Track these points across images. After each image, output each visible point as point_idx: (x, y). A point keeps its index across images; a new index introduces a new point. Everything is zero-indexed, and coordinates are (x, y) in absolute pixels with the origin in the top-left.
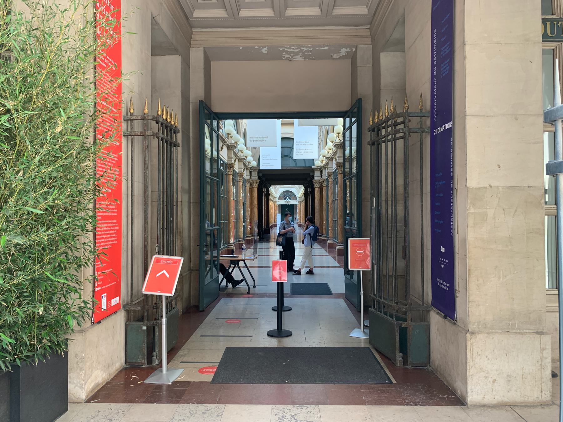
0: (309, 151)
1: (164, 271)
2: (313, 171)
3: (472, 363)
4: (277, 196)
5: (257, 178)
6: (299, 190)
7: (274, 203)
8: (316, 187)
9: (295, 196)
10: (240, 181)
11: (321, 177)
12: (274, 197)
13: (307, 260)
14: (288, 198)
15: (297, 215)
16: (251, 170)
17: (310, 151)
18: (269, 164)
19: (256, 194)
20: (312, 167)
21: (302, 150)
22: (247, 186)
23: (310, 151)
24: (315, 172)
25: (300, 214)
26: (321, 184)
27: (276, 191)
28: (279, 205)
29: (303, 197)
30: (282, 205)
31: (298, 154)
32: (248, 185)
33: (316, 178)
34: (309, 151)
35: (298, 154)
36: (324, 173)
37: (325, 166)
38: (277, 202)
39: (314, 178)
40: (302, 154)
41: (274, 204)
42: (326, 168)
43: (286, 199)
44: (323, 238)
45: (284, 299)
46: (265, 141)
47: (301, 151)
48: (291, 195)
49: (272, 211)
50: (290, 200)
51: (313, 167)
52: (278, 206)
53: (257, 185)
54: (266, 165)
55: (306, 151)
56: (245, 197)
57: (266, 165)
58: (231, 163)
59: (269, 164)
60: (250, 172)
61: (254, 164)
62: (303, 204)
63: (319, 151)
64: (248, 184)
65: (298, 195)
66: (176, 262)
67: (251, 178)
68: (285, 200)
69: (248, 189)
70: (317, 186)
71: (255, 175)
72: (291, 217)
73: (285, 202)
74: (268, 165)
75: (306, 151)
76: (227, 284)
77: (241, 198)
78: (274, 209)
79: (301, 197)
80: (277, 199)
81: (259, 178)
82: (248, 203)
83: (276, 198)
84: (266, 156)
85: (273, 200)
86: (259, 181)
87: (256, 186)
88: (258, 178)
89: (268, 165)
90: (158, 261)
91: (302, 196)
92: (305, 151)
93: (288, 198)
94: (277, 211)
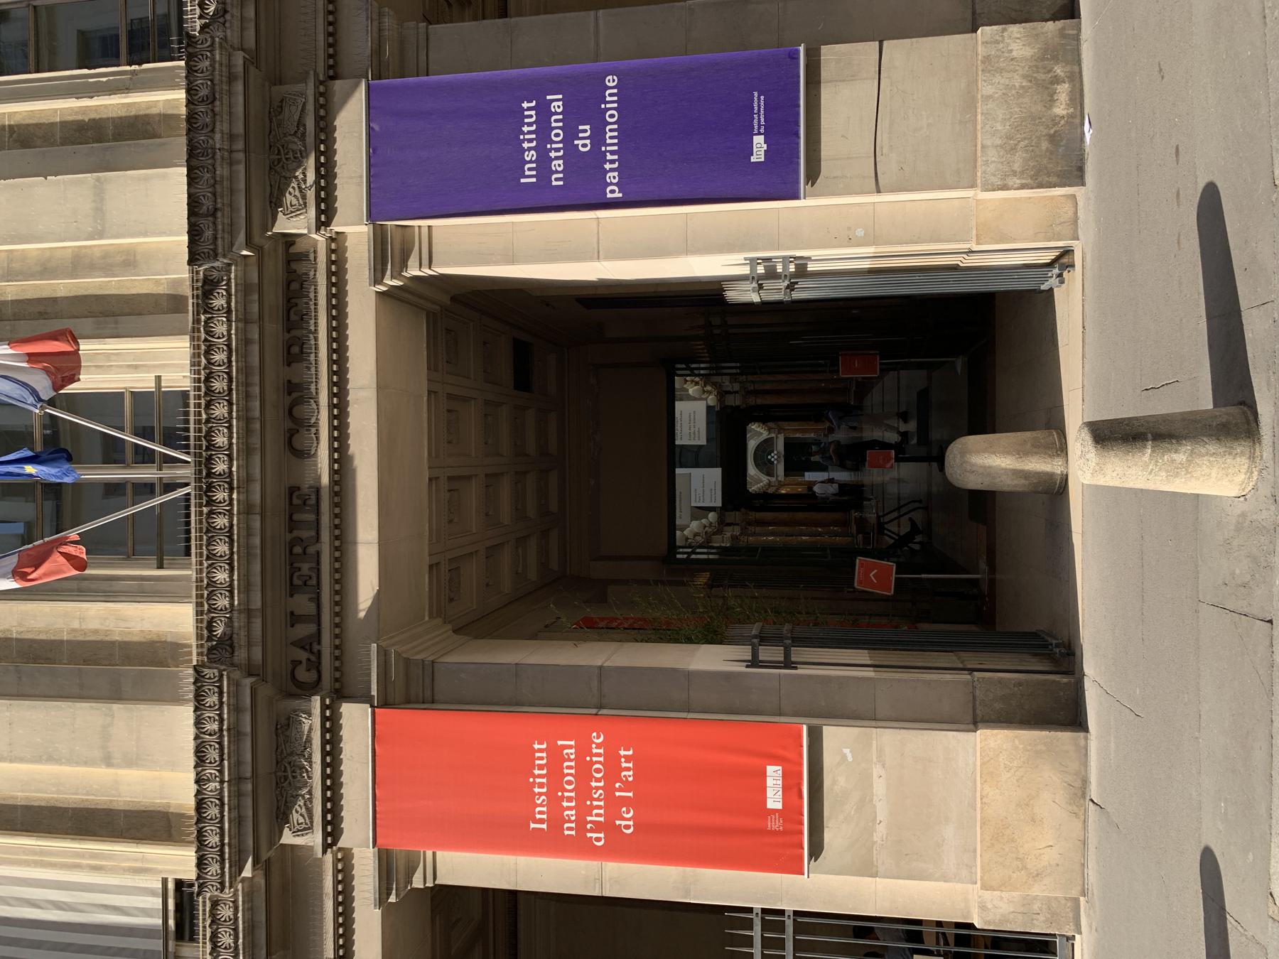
0: (692, 417)
1: (871, 575)
2: (724, 408)
3: (633, 633)
4: (765, 479)
5: (737, 513)
6: (757, 434)
7: (781, 485)
8: (754, 402)
9: (766, 441)
10: (746, 541)
11: (736, 392)
12: (769, 484)
13: (885, 422)
14: (769, 457)
15: (807, 436)
16: (722, 523)
17: (692, 415)
18: (711, 490)
19: (768, 516)
20: (718, 411)
21: (690, 430)
22: (754, 530)
23: (692, 415)
24: (727, 404)
25: (806, 432)
26: (749, 393)
27: (756, 479)
28: (786, 475)
29: (771, 424)
30: (786, 470)
31: (697, 435)
32: (752, 529)
33: (738, 403)
34: (692, 417)
35: (697, 435)
36: (729, 389)
37: (716, 386)
38: (779, 479)
39: (738, 407)
40: (697, 429)
41: (785, 485)
42: (720, 385)
43: (773, 459)
44: (854, 388)
45: (676, 402)
46: (680, 493)
47: (692, 431)
48: (766, 447)
49: (800, 490)
50: (775, 452)
51: (717, 409)
52: (787, 479)
53: (750, 513)
54: (713, 496)
55: (692, 421)
56: (772, 534)
57: (713, 496)
58: (732, 537)
59: (711, 490)
60: (729, 525)
61: (712, 516)
62: (786, 425)
63: (695, 399)
64: (750, 529)
65: (765, 435)
66: (862, 565)
67: (737, 524)
68: (775, 462)
69: (758, 529)
70: (752, 401)
71: (733, 516)
72: (813, 447)
73: (778, 462)
74: (713, 491)
75: (692, 421)
76: (916, 543)
77: (778, 539)
78: (796, 485)
79: (770, 430)
80: (773, 479)
81: (737, 509)
82: (786, 529)
83: (770, 482)
84: (698, 496)
85: (775, 488)
86: (743, 510)
87: (754, 515)
88: (737, 511)
89: (713, 491)
90: (860, 583)
91: (766, 425)
92: (692, 424)
93: (769, 457)
94: (800, 479)
